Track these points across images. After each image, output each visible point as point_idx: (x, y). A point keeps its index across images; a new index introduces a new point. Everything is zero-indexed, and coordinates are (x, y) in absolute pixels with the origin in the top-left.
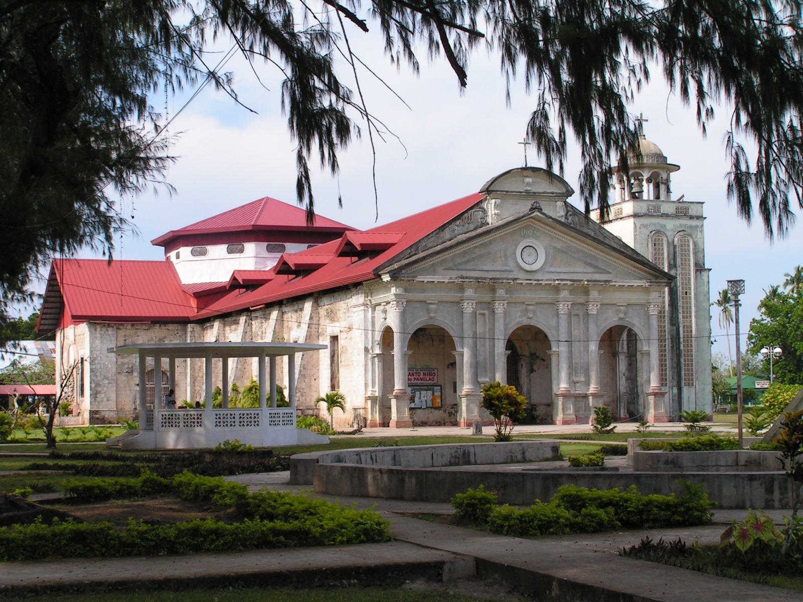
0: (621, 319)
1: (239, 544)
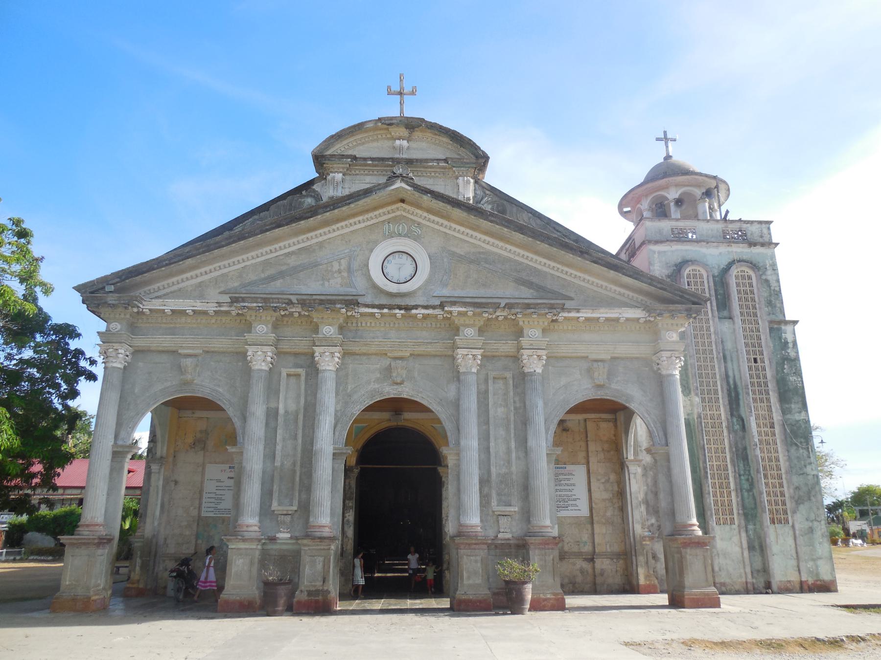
0: (599, 387)
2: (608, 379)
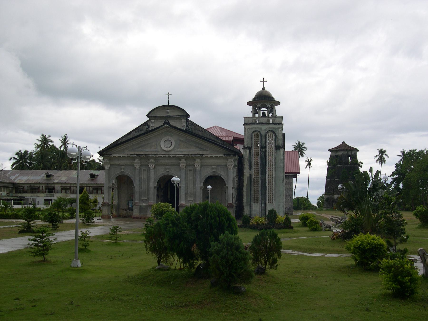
0: (214, 172)
1: (371, 247)
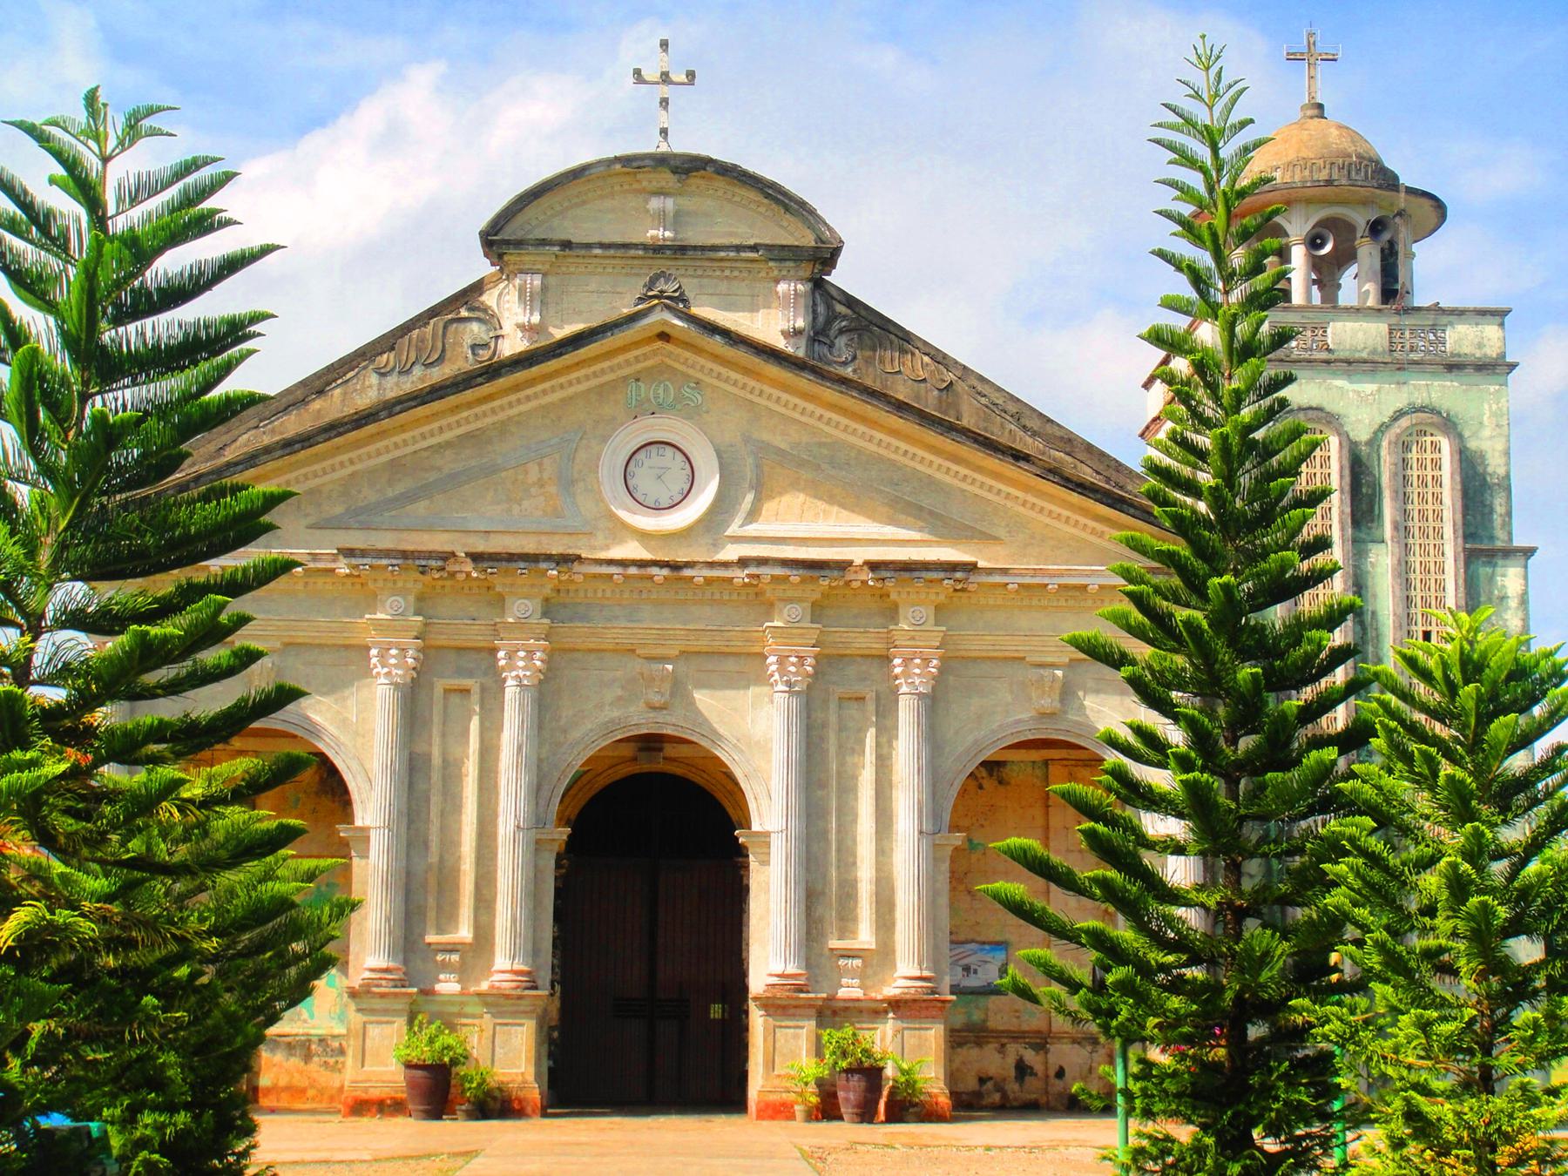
0: (1043, 715)
2: (1062, 700)
